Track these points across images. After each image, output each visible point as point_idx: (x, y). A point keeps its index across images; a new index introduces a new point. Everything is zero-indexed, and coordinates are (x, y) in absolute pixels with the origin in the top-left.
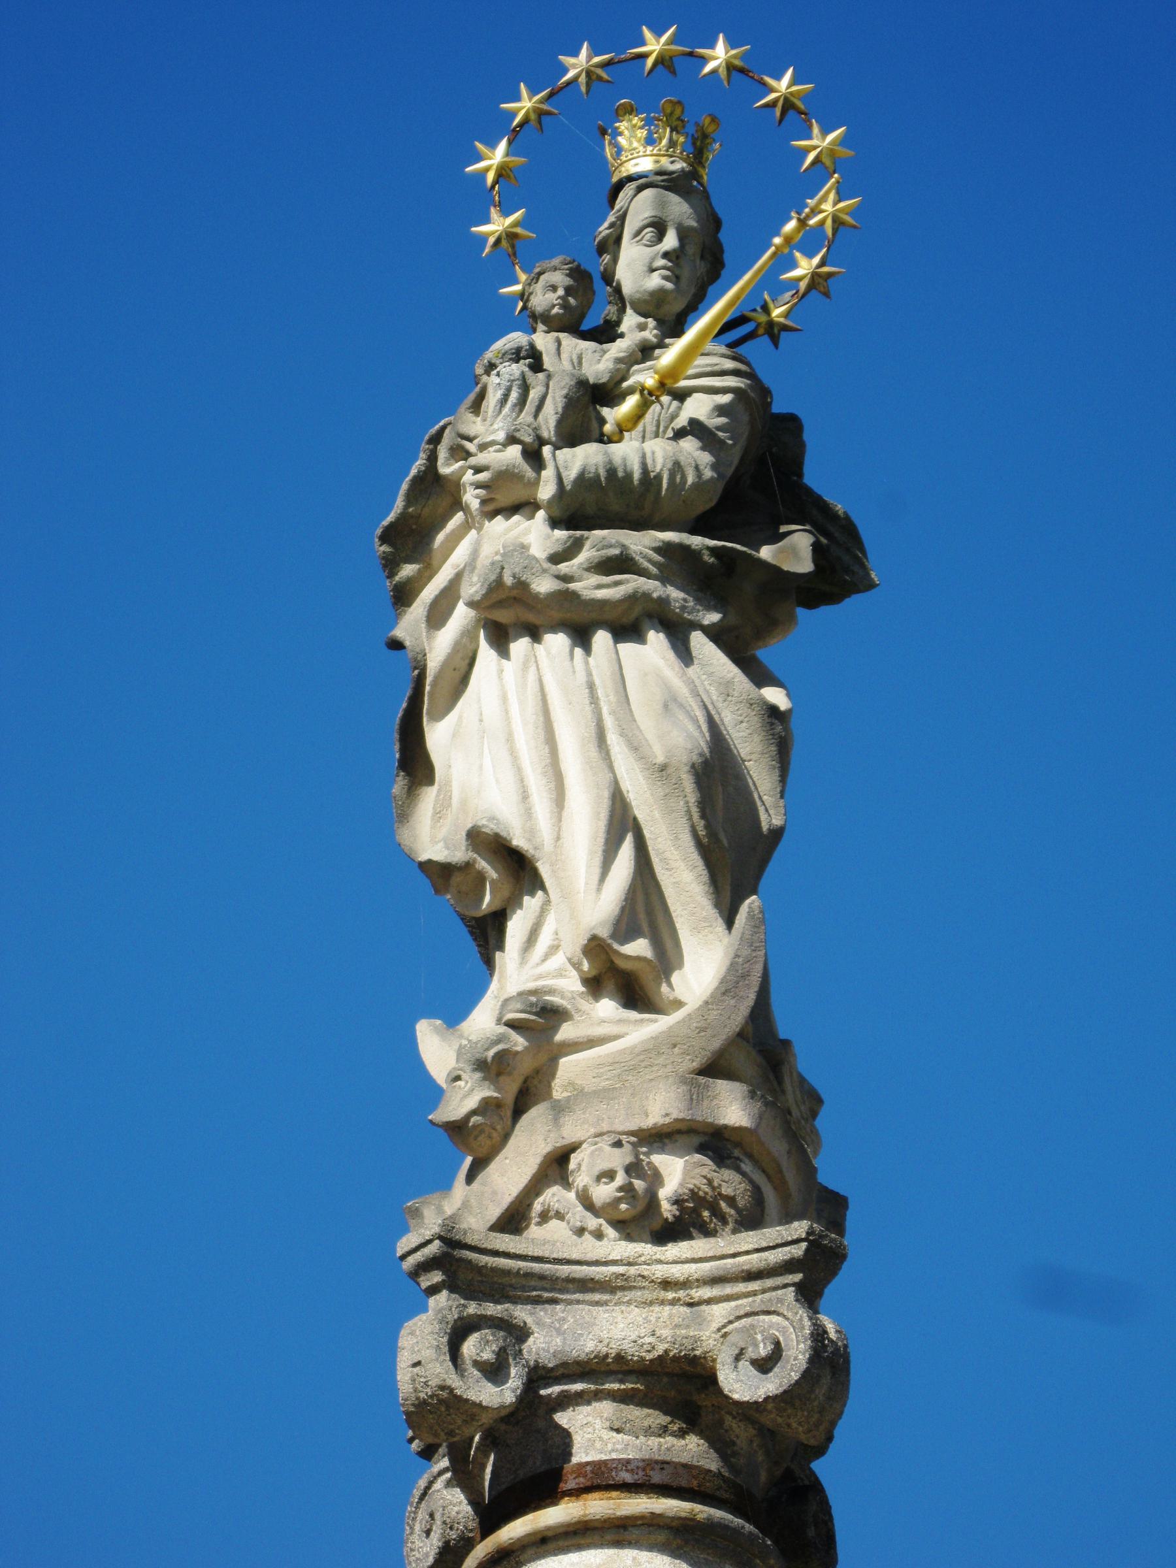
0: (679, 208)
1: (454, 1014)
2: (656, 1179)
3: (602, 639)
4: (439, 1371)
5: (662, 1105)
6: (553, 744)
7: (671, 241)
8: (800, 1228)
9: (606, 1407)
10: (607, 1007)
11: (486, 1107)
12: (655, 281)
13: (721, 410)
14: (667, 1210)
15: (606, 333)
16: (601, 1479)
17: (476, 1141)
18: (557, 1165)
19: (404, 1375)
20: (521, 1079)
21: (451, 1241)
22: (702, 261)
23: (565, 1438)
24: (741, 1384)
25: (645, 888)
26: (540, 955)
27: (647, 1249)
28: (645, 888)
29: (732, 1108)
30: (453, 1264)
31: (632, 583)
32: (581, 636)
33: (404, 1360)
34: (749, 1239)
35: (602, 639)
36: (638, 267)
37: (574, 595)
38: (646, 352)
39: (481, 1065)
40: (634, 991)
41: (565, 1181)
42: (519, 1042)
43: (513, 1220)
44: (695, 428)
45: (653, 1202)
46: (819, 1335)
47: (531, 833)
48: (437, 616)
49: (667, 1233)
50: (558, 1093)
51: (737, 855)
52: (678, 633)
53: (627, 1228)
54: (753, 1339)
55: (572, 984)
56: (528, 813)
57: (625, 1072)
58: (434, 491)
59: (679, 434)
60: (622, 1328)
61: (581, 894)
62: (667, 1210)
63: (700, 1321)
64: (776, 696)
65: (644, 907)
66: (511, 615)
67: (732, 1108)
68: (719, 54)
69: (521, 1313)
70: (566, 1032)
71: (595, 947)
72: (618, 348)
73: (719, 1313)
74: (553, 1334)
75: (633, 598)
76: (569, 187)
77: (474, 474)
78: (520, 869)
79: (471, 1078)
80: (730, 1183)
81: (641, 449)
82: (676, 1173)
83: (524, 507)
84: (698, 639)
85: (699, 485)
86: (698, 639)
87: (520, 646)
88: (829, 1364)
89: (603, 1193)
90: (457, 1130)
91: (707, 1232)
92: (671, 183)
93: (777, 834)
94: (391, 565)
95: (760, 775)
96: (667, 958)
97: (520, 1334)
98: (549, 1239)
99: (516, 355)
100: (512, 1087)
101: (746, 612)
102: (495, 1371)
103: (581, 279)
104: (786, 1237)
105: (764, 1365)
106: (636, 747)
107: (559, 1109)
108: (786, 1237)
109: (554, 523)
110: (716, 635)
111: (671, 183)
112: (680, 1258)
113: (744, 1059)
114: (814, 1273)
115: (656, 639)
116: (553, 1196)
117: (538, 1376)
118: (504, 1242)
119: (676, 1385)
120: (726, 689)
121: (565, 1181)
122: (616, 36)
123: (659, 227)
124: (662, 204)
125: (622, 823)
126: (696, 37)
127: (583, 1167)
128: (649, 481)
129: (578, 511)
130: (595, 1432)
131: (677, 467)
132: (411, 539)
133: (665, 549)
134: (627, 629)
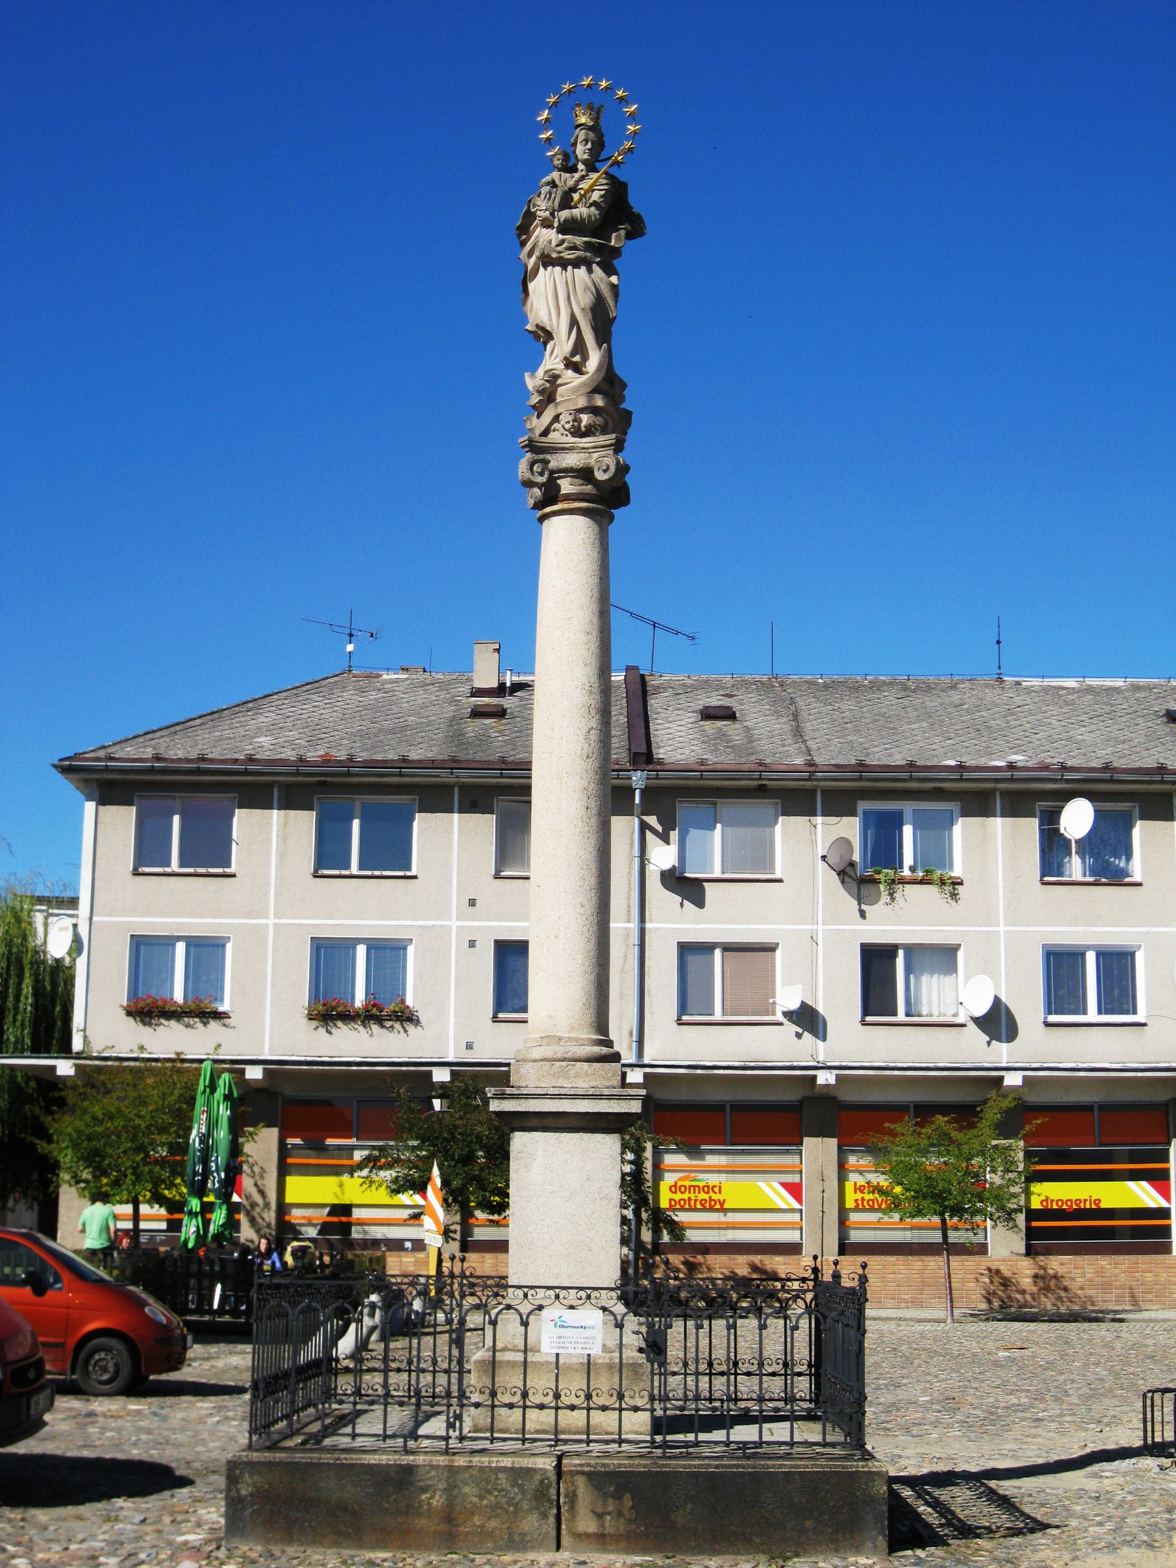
0: (591, 135)
1: (533, 370)
2: (580, 421)
3: (570, 268)
4: (528, 475)
5: (582, 402)
6: (556, 298)
7: (589, 146)
8: (614, 436)
9: (569, 479)
10: (570, 373)
11: (540, 401)
12: (586, 156)
13: (602, 196)
14: (583, 429)
15: (573, 170)
16: (568, 498)
17: (539, 409)
18: (556, 419)
19: (520, 475)
20: (548, 396)
21: (531, 441)
22: (598, 146)
23: (559, 487)
24: (600, 476)
25: (580, 339)
26: (553, 359)
27: (578, 440)
28: (580, 339)
29: (599, 402)
30: (532, 446)
31: (579, 253)
32: (564, 268)
33: (520, 471)
34: (602, 438)
35: (570, 268)
36: (582, 151)
37: (562, 258)
38: (583, 178)
39: (538, 391)
40: (577, 368)
41: (558, 422)
42: (548, 385)
43: (545, 433)
44: (595, 204)
45: (579, 426)
46: (618, 462)
47: (551, 325)
48: (530, 254)
49: (583, 435)
50: (559, 399)
51: (603, 332)
52: (588, 265)
53: (574, 434)
54: (603, 464)
55: (562, 366)
56: (551, 319)
57: (573, 389)
58: (529, 216)
59: (591, 205)
60: (572, 460)
61: (562, 345)
62: (583, 429)
63: (591, 457)
64: (614, 279)
65: (579, 347)
66: (547, 261)
67: (599, 402)
68: (604, 84)
69: (548, 457)
70: (559, 381)
71: (566, 358)
72: (577, 176)
73: (595, 455)
74: (555, 462)
75: (576, 258)
76: (563, 124)
77: (269, 1209)
78: (549, 336)
79: (536, 395)
80: (599, 420)
81: (581, 211)
82: (585, 419)
83: (550, 226)
84: (594, 266)
85: (596, 220)
86: (594, 266)
87: (550, 268)
88: (623, 469)
89: (568, 426)
90: (534, 407)
91: (594, 435)
92: (590, 128)
93: (615, 318)
94: (519, 236)
95: (610, 301)
96: (585, 358)
97: (546, 462)
98: (555, 437)
99: (548, 184)
100: (546, 395)
101: (607, 259)
102: (541, 474)
103: (566, 157)
104: (610, 438)
105: (605, 471)
106: (578, 302)
107: (557, 405)
108: (610, 438)
109: (558, 232)
110: (598, 264)
111: (590, 128)
112: (586, 442)
113: (605, 387)
114: (618, 447)
115: (583, 268)
116: (556, 425)
117: (552, 472)
118: (543, 439)
119: (585, 474)
120: (601, 279)
121: (558, 422)
122: (576, 79)
123: (586, 141)
124: (587, 134)
125: (574, 322)
126: (598, 78)
127: (564, 418)
128: (582, 220)
129: (567, 228)
130: (566, 486)
131: (590, 216)
132: (524, 230)
133: (585, 243)
134: (576, 263)
